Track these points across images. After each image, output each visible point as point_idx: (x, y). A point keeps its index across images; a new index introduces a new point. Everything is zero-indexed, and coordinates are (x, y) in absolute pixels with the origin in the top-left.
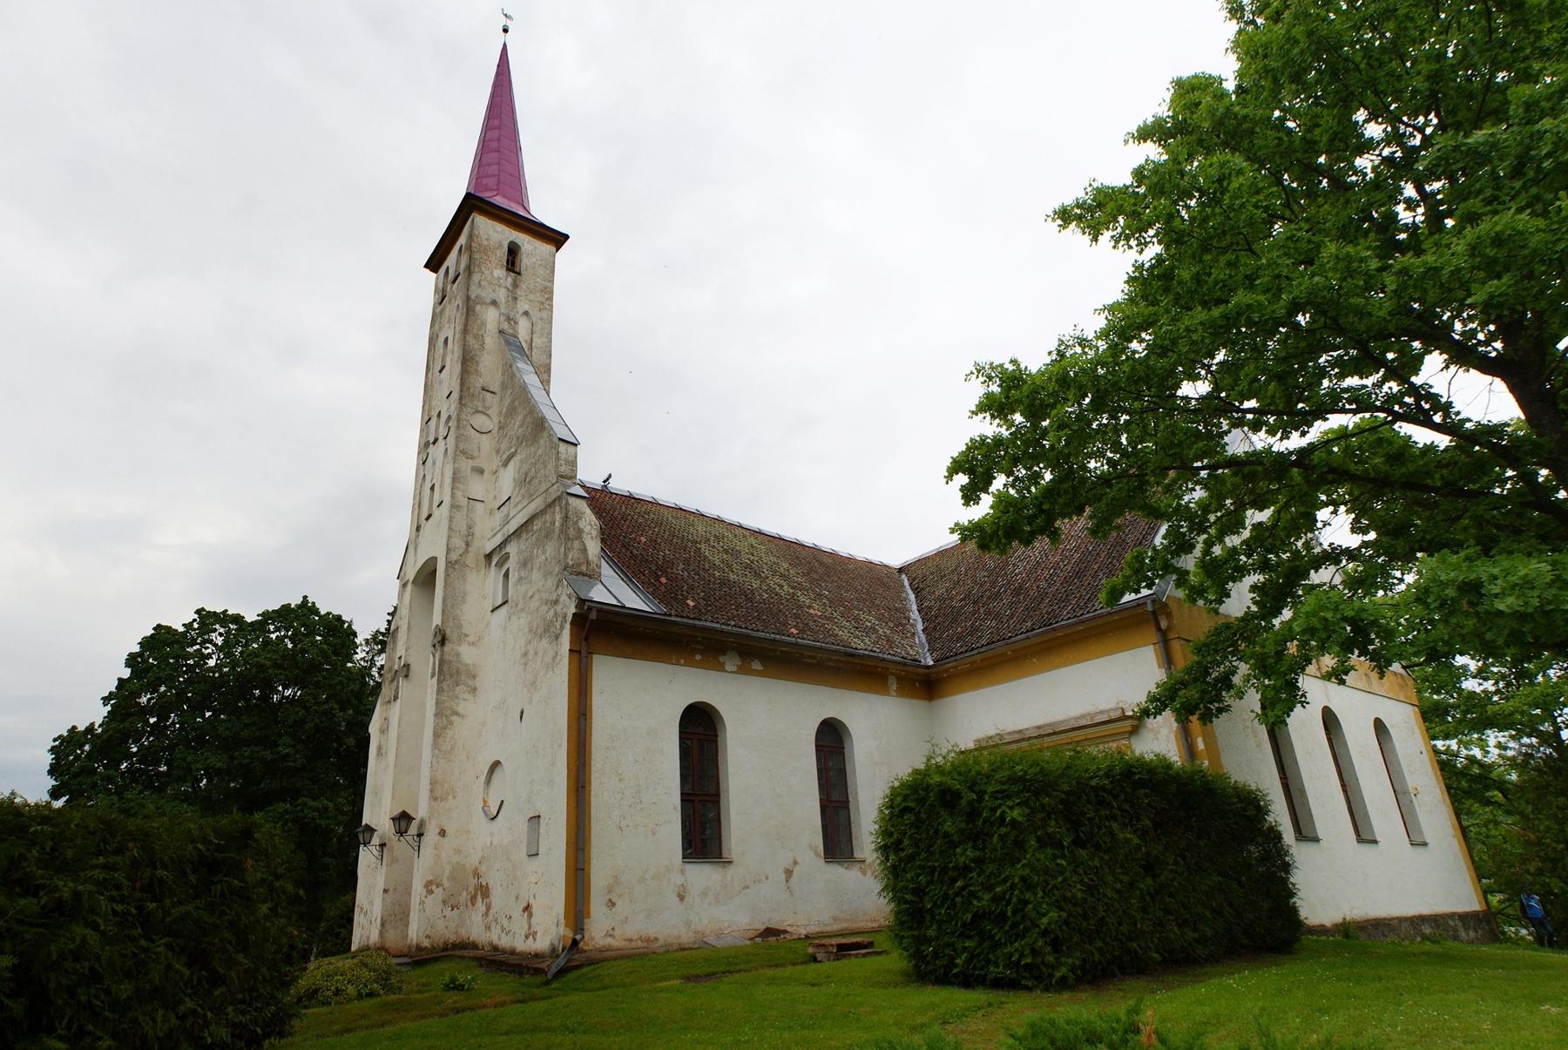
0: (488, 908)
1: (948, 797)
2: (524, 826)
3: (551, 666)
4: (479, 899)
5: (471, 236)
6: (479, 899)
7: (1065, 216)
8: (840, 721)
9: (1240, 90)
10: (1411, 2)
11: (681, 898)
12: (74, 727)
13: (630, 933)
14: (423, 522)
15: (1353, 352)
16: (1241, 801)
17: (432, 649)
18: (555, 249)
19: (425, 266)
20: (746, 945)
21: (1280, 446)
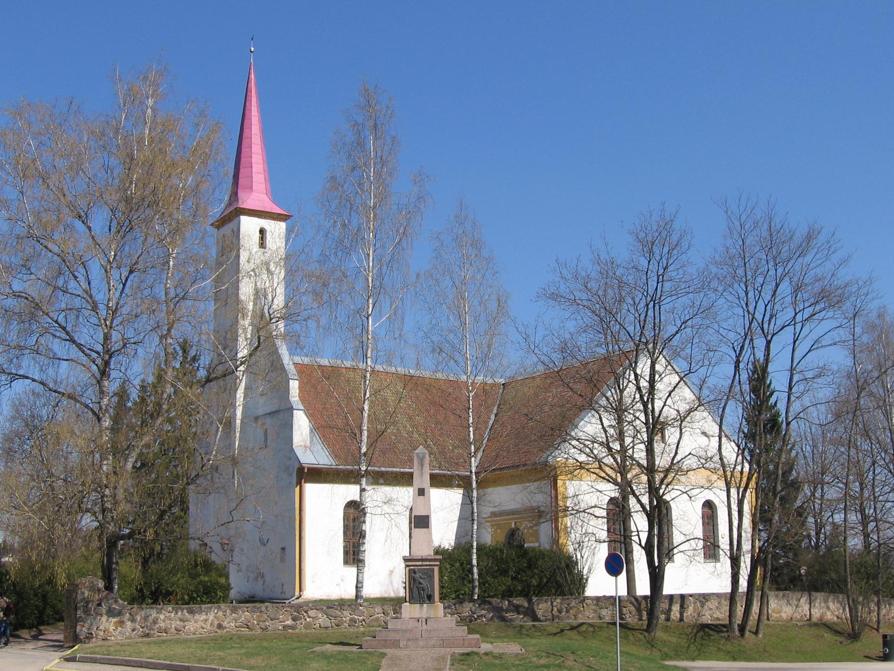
0: (264, 582)
4: (260, 579)
6: (260, 579)
11: (343, 580)
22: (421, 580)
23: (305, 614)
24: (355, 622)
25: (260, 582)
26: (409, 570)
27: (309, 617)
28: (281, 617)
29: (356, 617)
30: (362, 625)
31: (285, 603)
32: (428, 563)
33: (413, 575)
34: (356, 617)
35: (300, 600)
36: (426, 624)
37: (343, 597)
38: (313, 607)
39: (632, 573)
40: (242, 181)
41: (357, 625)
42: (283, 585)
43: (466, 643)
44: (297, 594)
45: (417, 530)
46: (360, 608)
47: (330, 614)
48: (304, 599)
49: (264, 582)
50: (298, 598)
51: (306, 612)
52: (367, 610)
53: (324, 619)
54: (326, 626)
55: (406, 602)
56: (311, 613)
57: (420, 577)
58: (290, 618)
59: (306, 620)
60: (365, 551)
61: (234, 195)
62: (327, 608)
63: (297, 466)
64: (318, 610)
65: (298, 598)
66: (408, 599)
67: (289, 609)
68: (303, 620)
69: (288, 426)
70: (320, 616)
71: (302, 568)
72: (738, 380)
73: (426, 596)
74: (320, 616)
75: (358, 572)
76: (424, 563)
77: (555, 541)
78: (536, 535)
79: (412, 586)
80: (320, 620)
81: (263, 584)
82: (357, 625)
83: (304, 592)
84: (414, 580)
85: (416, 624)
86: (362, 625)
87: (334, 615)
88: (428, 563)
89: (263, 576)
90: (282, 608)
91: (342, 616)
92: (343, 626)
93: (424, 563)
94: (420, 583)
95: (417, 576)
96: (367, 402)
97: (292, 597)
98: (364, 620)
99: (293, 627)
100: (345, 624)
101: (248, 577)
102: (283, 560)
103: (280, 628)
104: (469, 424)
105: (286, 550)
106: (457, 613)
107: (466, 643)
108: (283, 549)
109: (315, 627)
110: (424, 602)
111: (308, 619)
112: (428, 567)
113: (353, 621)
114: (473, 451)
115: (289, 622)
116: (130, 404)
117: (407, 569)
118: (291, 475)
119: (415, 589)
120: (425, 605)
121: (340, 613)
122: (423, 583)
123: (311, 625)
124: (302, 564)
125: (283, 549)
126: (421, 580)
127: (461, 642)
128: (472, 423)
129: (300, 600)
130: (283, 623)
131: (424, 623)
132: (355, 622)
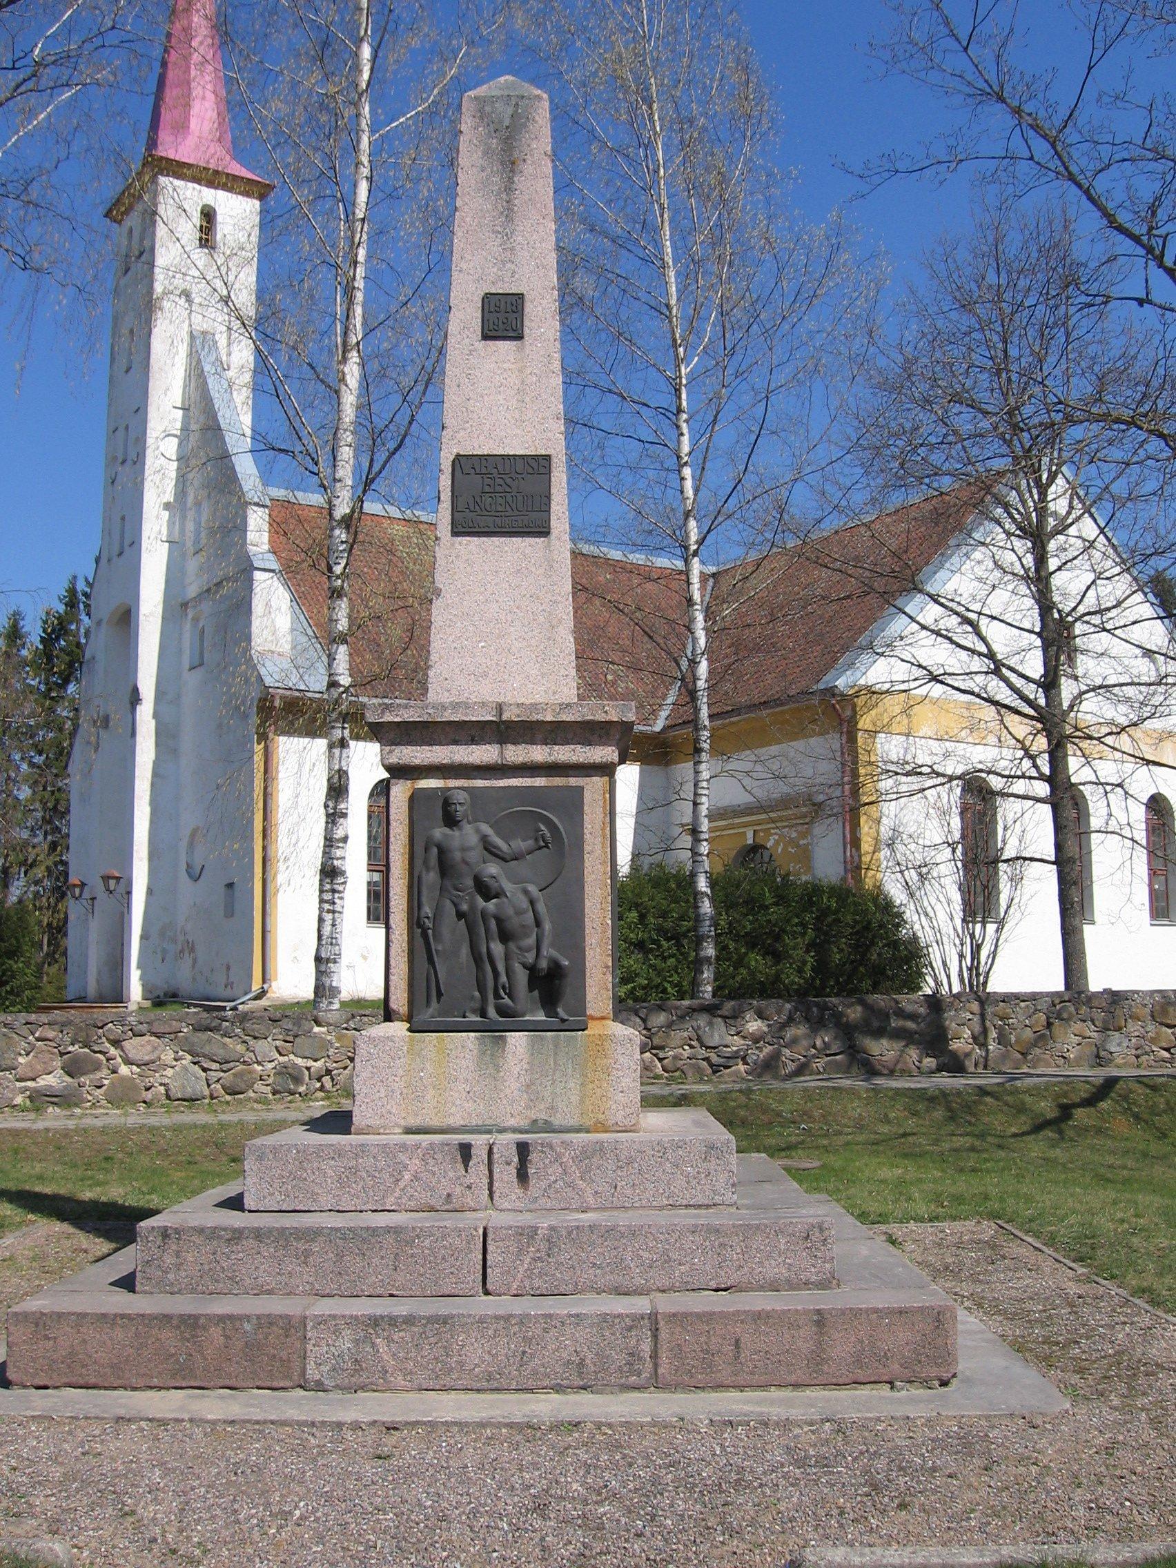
0: (195, 961)
1: (1154, 830)
2: (223, 890)
3: (170, 271)
4: (186, 954)
5: (33, 1222)
6: (186, 954)
7: (112, 1284)
8: (1166, 799)
9: (831, 691)
10: (1172, 1101)
11: (365, 958)
12: (1093, 922)
13: (158, 322)
14: (126, 547)
15: (382, 117)
16: (781, 899)
17: (878, 1212)
18: (834, 741)
19: (520, 337)
20: (1061, 704)
21: (35, 1127)
22: (493, 869)
23: (113, 1051)
24: (297, 1080)
25: (188, 960)
26: (415, 799)
27: (128, 1062)
28: (21, 1060)
29: (299, 1061)
30: (322, 1088)
31: (224, 1008)
32: (538, 754)
33: (439, 832)
34: (299, 1061)
35: (264, 1002)
36: (523, 1176)
37: (362, 995)
38: (144, 1028)
39: (1078, 937)
40: (166, 116)
41: (302, 1089)
42: (228, 968)
43: (841, 1346)
44: (256, 986)
45: (472, 544)
46: (316, 1029)
47: (207, 1050)
48: (273, 999)
49: (195, 961)
50: (258, 997)
51: (116, 1043)
52: (339, 1039)
53: (185, 1068)
54: (189, 1092)
55: (389, 1016)
56: (134, 1047)
57: (489, 848)
58: (58, 1063)
59: (114, 1072)
60: (345, 839)
61: (152, 143)
62: (195, 1030)
63: (255, 693)
64: (158, 1036)
65: (258, 997)
66: (399, 1002)
67: (51, 1034)
68: (105, 1072)
69: (240, 608)
70: (168, 1056)
71: (268, 928)
72: (1023, 681)
73: (522, 976)
74: (168, 1056)
75: (321, 910)
76: (517, 754)
77: (855, 868)
78: (806, 856)
79: (427, 910)
80: (170, 1072)
81: (193, 966)
82: (302, 1089)
83: (274, 984)
84: (445, 867)
85: (449, 1175)
86: (322, 1088)
87: (221, 1053)
88: (538, 754)
89: (192, 950)
90: (25, 1030)
91: (249, 1056)
92: (251, 1094)
93: (517, 754)
94: (485, 889)
95: (467, 837)
96: (354, 357)
97: (246, 994)
98: (329, 1072)
99: (63, 1099)
100: (259, 1086)
101: (164, 951)
102: (230, 912)
103: (19, 1100)
104: (679, 457)
105: (236, 886)
106: (653, 1048)
107: (841, 1346)
108: (230, 886)
109: (148, 1096)
110: (509, 1020)
111: (124, 1070)
112: (540, 782)
113: (291, 1075)
114: (694, 537)
115: (53, 1080)
116: (24, 652)
117: (400, 792)
118: (245, 716)
119: (451, 932)
120: (517, 1041)
121: (240, 1048)
122: (508, 886)
123: (135, 1088)
124: (268, 921)
125: (230, 886)
126: (493, 869)
127: (804, 1341)
128: (690, 454)
129: (264, 1002)
130: (30, 1084)
131: (506, 1174)
132: (297, 1080)
